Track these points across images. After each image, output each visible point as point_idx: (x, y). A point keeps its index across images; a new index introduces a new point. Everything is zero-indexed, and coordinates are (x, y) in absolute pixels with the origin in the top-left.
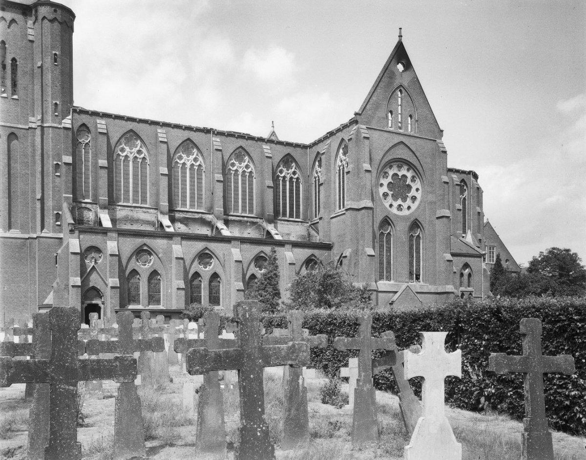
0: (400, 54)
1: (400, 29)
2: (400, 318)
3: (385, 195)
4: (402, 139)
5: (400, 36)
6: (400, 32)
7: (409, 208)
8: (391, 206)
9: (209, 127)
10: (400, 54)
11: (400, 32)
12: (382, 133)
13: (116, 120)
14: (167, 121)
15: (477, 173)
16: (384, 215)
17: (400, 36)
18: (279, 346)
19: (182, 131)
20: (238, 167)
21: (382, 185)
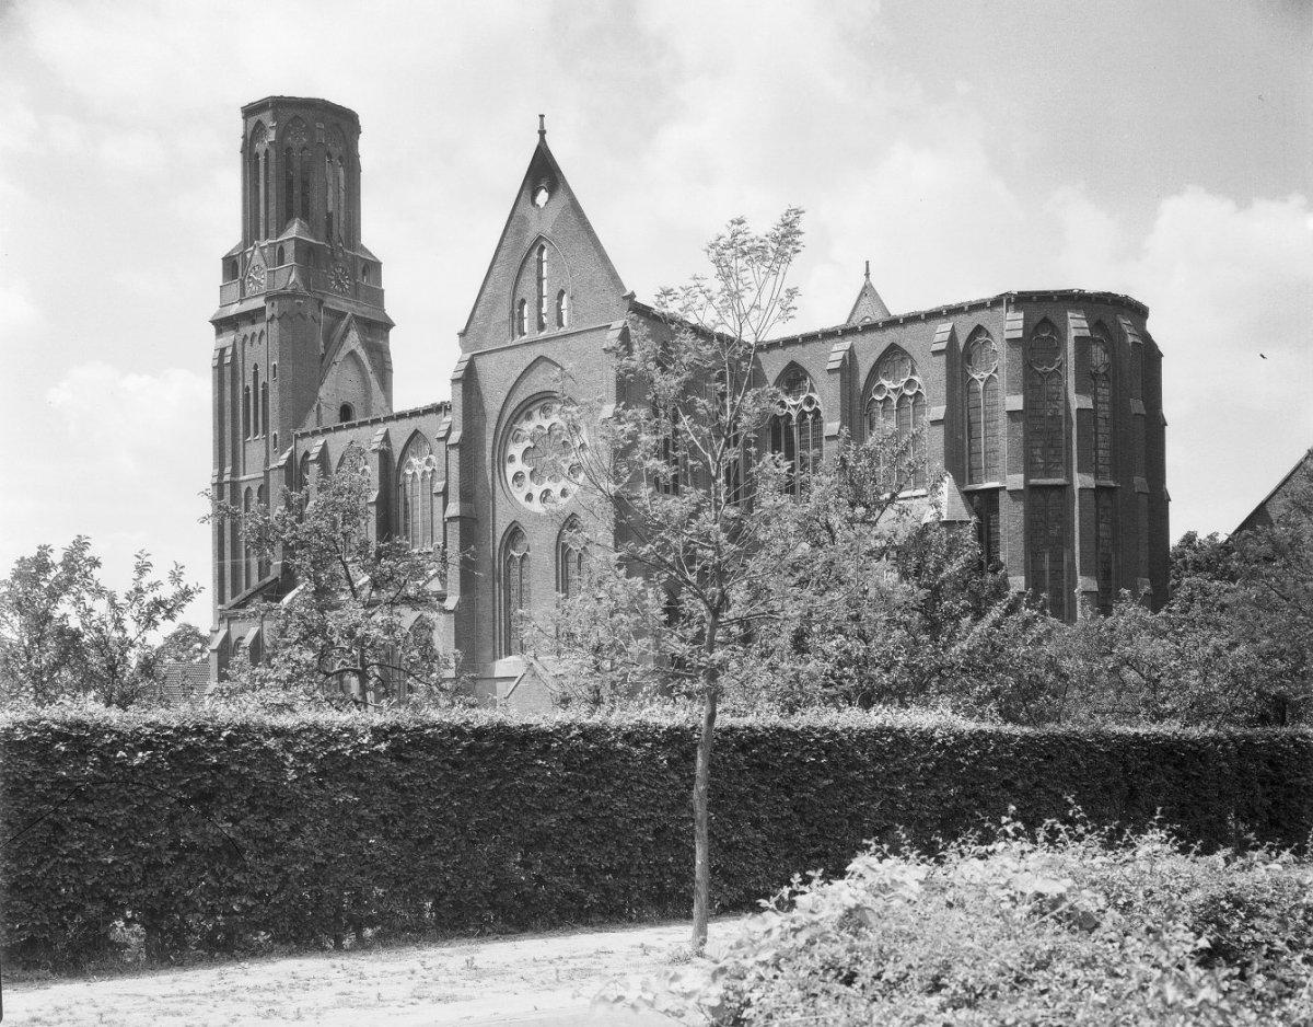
0: (543, 172)
1: (542, 116)
2: (118, 736)
3: (518, 477)
4: (539, 350)
5: (542, 133)
6: (542, 125)
7: (564, 493)
8: (529, 497)
9: (438, 402)
10: (543, 172)
11: (542, 125)
12: (504, 353)
13: (337, 433)
14: (954, 301)
15: (1137, 296)
16: (509, 522)
17: (542, 133)
18: (1008, 728)
19: (988, 312)
20: (889, 393)
21: (512, 459)
